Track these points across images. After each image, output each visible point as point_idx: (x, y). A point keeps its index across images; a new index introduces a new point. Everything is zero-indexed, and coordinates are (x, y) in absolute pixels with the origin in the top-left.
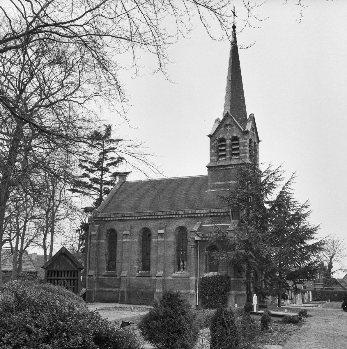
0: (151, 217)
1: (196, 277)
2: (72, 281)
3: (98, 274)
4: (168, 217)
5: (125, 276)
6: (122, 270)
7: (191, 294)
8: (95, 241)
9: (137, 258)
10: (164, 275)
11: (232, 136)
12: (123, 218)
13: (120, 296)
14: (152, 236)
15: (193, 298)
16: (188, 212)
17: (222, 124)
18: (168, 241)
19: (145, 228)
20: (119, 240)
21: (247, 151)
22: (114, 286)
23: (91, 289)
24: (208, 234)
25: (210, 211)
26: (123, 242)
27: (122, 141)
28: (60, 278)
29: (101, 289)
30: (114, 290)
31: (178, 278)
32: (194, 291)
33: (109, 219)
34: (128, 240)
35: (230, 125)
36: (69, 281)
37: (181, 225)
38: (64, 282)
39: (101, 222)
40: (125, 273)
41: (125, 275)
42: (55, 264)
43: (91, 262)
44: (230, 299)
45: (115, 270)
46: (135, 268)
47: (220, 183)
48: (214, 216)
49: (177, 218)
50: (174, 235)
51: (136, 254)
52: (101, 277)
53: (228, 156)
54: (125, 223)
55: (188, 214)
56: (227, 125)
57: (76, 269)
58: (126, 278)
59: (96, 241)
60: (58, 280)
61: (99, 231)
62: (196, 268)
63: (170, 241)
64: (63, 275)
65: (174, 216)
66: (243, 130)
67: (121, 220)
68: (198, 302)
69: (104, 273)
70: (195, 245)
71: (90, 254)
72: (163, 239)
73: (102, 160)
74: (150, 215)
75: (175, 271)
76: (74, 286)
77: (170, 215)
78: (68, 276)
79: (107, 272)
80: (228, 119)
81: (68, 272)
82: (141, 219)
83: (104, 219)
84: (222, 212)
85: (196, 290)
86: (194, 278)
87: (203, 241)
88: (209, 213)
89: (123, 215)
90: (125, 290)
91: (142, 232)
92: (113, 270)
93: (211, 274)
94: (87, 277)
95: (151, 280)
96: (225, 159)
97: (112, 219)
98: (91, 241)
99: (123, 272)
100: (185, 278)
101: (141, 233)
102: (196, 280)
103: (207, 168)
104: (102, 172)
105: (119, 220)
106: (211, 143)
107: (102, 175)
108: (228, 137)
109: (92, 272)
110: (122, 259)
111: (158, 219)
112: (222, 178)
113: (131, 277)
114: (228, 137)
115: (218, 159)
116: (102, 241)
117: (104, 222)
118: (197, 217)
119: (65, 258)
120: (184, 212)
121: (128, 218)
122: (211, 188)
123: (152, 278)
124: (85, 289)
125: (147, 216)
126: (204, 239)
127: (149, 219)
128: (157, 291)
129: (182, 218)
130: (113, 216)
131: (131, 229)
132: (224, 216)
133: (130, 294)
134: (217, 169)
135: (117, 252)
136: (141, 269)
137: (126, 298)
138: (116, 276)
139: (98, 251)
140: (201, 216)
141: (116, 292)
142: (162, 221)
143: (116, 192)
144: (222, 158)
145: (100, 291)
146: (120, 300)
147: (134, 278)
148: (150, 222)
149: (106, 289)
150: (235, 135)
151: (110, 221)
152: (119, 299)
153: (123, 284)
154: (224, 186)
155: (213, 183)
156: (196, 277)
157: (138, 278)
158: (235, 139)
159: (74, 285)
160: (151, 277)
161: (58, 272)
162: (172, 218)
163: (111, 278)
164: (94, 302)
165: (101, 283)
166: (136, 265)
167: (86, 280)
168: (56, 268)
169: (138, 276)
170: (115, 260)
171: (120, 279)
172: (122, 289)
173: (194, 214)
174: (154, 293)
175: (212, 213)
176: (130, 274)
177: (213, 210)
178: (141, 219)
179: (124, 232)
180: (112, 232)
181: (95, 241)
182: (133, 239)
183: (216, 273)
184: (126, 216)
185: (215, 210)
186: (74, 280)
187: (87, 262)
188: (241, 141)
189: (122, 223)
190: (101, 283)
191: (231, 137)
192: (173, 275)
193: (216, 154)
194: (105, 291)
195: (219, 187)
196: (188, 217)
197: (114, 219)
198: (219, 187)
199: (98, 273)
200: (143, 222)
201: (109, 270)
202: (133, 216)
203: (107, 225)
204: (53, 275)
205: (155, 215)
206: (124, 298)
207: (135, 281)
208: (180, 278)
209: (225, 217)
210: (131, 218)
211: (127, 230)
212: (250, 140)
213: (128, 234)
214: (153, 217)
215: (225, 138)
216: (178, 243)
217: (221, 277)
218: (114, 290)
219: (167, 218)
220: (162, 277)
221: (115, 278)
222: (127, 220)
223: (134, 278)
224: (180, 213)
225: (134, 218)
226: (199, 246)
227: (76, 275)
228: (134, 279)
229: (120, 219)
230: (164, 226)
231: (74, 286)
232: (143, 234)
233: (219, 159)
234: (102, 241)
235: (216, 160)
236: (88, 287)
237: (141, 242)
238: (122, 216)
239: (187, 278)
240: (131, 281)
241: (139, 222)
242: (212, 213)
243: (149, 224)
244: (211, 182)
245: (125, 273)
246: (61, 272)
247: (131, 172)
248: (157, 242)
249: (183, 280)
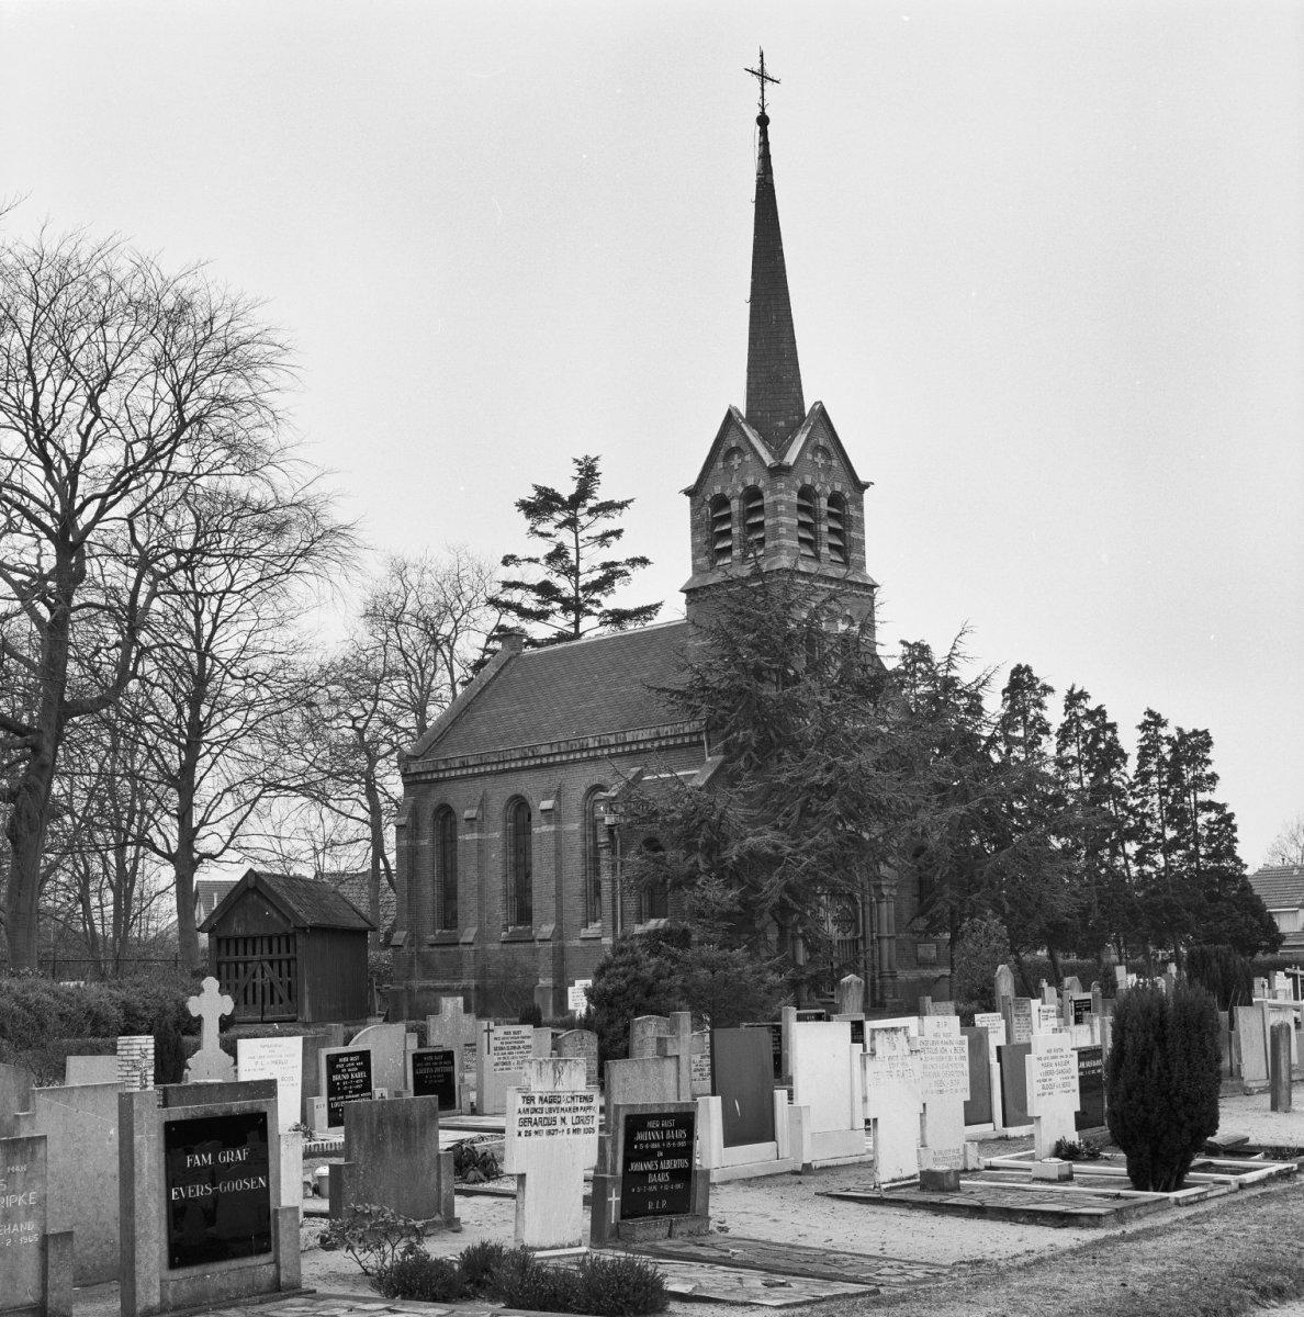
0: (526, 763)
2: (284, 965)
5: (471, 944)
10: (559, 934)
11: (743, 484)
17: (725, 448)
21: (783, 530)
25: (658, 733)
27: (630, 505)
28: (250, 957)
33: (435, 776)
35: (824, 450)
36: (276, 965)
38: (263, 968)
39: (421, 787)
41: (470, 939)
42: (235, 919)
46: (497, 918)
48: (668, 748)
52: (425, 949)
53: (736, 552)
55: (610, 746)
56: (731, 452)
57: (291, 931)
58: (473, 948)
60: (245, 963)
62: (614, 913)
63: (573, 833)
64: (258, 950)
65: (578, 756)
66: (768, 460)
69: (431, 938)
70: (607, 840)
77: (567, 753)
78: (271, 952)
80: (733, 431)
81: (270, 939)
84: (686, 734)
88: (656, 739)
90: (473, 983)
97: (441, 775)
101: (510, 814)
103: (684, 596)
106: (694, 512)
107: (576, 624)
108: (734, 489)
114: (734, 489)
115: (713, 562)
117: (426, 786)
119: (261, 901)
120: (600, 742)
125: (519, 759)
127: (523, 769)
129: (595, 759)
143: (484, 689)
148: (525, 776)
150: (750, 482)
157: (505, 946)
158: (753, 494)
159: (289, 976)
161: (245, 940)
162: (575, 761)
163: (445, 949)
166: (498, 907)
168: (237, 929)
169: (504, 942)
174: (533, 988)
175: (663, 738)
177: (666, 729)
183: (663, 921)
186: (237, 964)
188: (768, 499)
191: (818, 488)
192: (584, 933)
193: (706, 548)
197: (447, 775)
200: (511, 778)
201: (446, 928)
203: (433, 793)
204: (232, 950)
205: (534, 757)
209: (689, 748)
212: (806, 493)
214: (532, 763)
215: (728, 493)
220: (548, 940)
223: (496, 946)
227: (291, 950)
235: (707, 567)
242: (663, 738)
243: (526, 785)
246: (254, 939)
247: (661, 604)
248: (541, 835)
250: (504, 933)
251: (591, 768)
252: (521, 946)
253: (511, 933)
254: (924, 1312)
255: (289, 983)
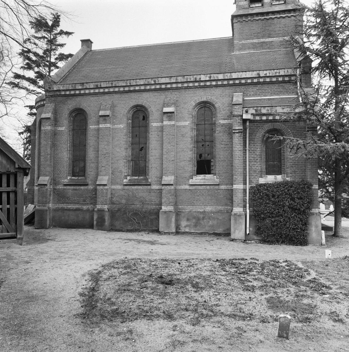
1: (245, 184)
3: (55, 182)
4: (180, 85)
6: (97, 175)
7: (235, 214)
8: (49, 128)
9: (124, 154)
10: (177, 183)
12: (97, 91)
13: (95, 217)
14: (150, 118)
15: (241, 220)
16: (218, 77)
18: (180, 126)
19: (136, 106)
20: (92, 127)
22: (84, 201)
23: (44, 206)
24: (266, 108)
25: (259, 74)
26: (98, 130)
29: (61, 206)
30: (85, 207)
31: (200, 187)
32: (241, 210)
33: (72, 92)
34: (108, 125)
37: (204, 99)
39: (60, 99)
40: (103, 179)
43: (42, 163)
44: (313, 223)
45: (84, 175)
46: (121, 172)
47: (255, 41)
48: (264, 83)
49: (196, 87)
50: (191, 116)
51: (123, 149)
52: (60, 187)
54: (102, 98)
57: (12, 170)
58: (106, 187)
59: (50, 129)
61: (55, 112)
63: (184, 127)
65: (191, 85)
67: (95, 94)
68: (250, 227)
69: (66, 181)
70: (242, 128)
71: (39, 149)
72: (173, 123)
73: (47, 52)
74: (147, 83)
75: (193, 175)
76: (8, 206)
78: (8, 185)
79: (70, 179)
82: (130, 91)
83: (63, 93)
84: (280, 76)
85: (245, 206)
86: (241, 186)
87: (257, 121)
89: (97, 86)
90: (106, 207)
91: (131, 112)
92: (81, 176)
93: (270, 179)
94: (36, 188)
95: (150, 191)
96: (260, 5)
97: (77, 92)
98: (42, 128)
99: (99, 178)
100: (212, 187)
102: (245, 190)
104: (49, 69)
105: (90, 94)
109: (44, 179)
110: (98, 157)
111: (161, 89)
112: (259, 33)
113: (113, 187)
116: (60, 129)
117: (65, 98)
118: (234, 85)
121: (106, 90)
122: (240, 49)
123: (152, 188)
124: (33, 206)
126: (258, 118)
128: (164, 208)
129: (205, 87)
130: (80, 87)
131: (113, 107)
132: (284, 82)
133: (113, 214)
134: (249, 19)
135: (88, 147)
136: (130, 173)
137: (106, 220)
138: (87, 185)
139: (54, 146)
140: (240, 83)
141: (88, 210)
142: (168, 93)
144: (255, 4)
145: (60, 209)
146: (97, 223)
147: (119, 187)
148: (145, 95)
149: (70, 206)
151: (75, 95)
152: (95, 223)
153: (100, 199)
154: (262, 45)
155: (243, 42)
156: (245, 184)
159: (8, 203)
160: (150, 185)
163: (78, 188)
164: (49, 228)
165: (60, 196)
167: (34, 192)
170: (84, 160)
171: (95, 190)
172: (99, 207)
173: (228, 80)
175: (262, 77)
176: (113, 182)
178: (130, 91)
179: (101, 113)
180: (78, 114)
181: (49, 128)
182: (117, 124)
183: (279, 178)
184: (102, 86)
185: (268, 73)
186: (8, 193)
187: (34, 174)
189: (96, 98)
190: (60, 196)
192: (191, 182)
194: (69, 210)
195: (254, 46)
196: (217, 86)
197: (82, 92)
198: (254, 46)
199: (54, 180)
200: (133, 95)
201: (73, 176)
202: (116, 87)
203: (69, 102)
205: (155, 84)
206: (103, 221)
207: (122, 193)
208: (203, 187)
210: (111, 90)
211: (105, 110)
213: (108, 116)
214: (153, 87)
216: (198, 130)
217: (292, 183)
218: (85, 207)
219: (177, 89)
220: (172, 185)
221: (86, 187)
222: (104, 93)
223: (119, 187)
224: (202, 80)
225: (117, 89)
226: (248, 130)
228: (119, 189)
229: (92, 91)
230: (172, 101)
231: (8, 206)
232: (133, 116)
233: (251, 6)
234: (60, 129)
235: (247, 6)
236: (39, 202)
237: (130, 128)
238: (97, 88)
239: (217, 187)
240: (113, 192)
241: (126, 95)
242: (262, 77)
244: (240, 40)
245: (103, 179)
249: (208, 190)
250: (125, 180)
251: (200, 92)
252: (140, 187)
253: (129, 180)
254: (257, 350)
255: (8, 209)
